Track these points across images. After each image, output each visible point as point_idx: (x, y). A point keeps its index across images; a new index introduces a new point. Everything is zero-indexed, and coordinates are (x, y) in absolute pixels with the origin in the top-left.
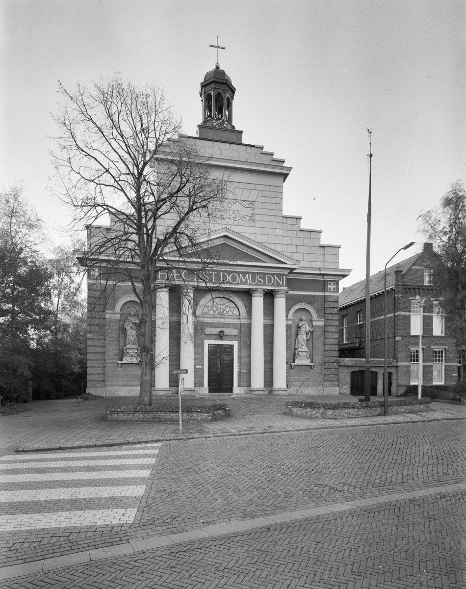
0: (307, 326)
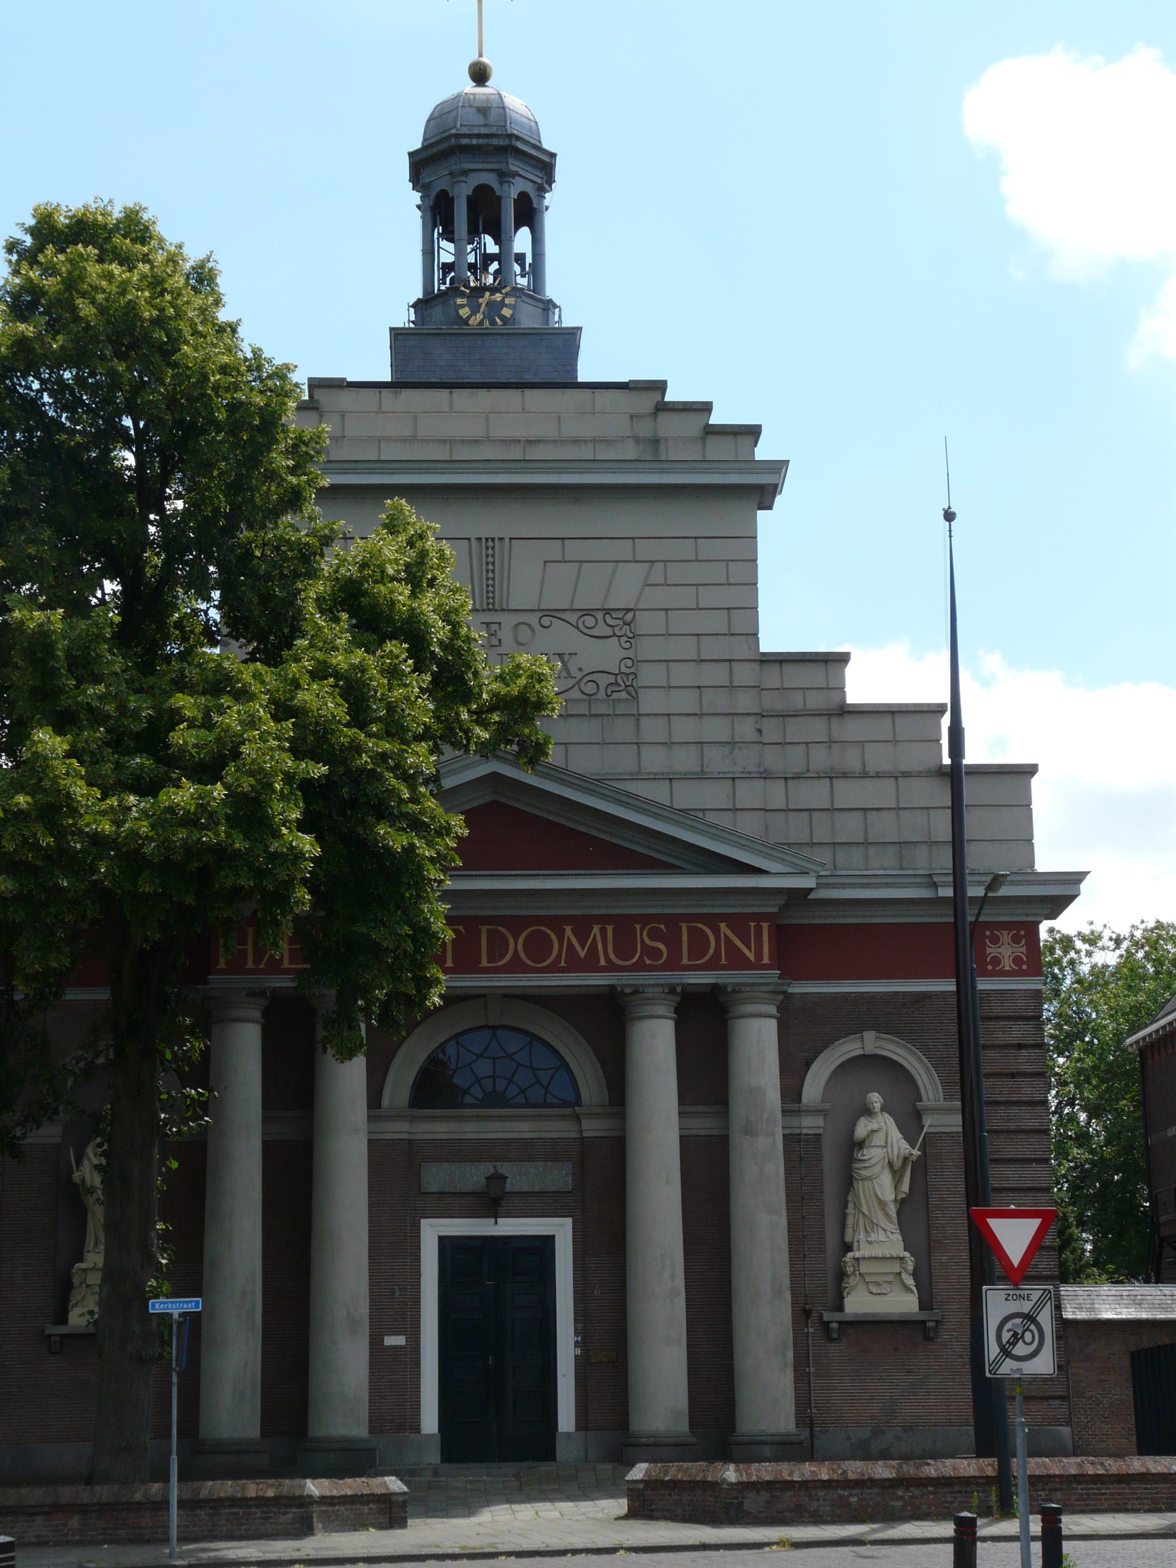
0: (896, 1135)
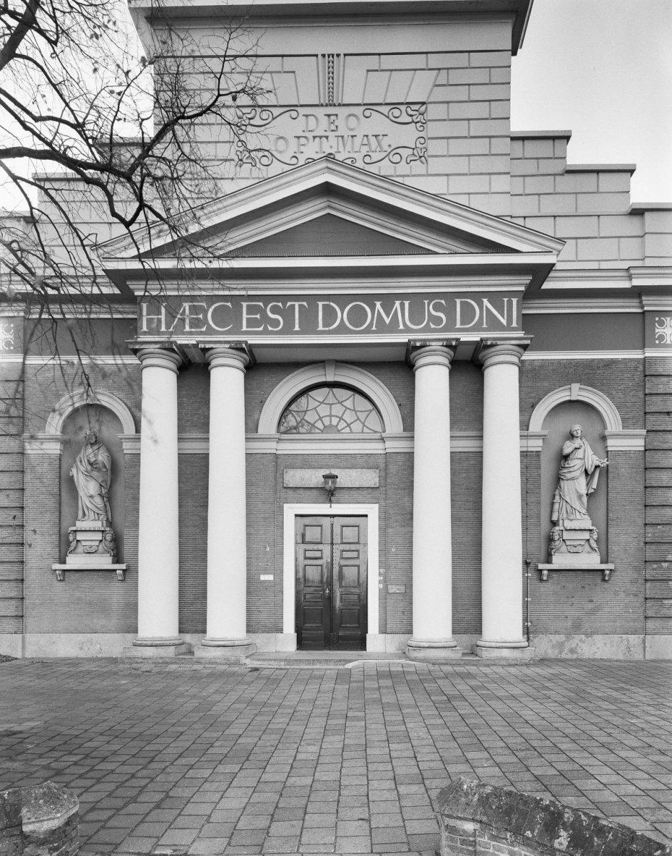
0: (589, 452)
